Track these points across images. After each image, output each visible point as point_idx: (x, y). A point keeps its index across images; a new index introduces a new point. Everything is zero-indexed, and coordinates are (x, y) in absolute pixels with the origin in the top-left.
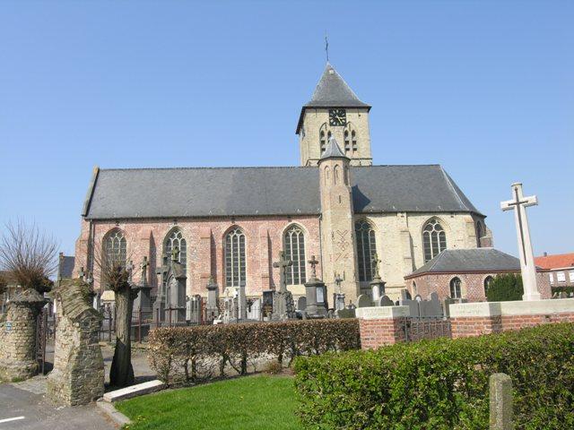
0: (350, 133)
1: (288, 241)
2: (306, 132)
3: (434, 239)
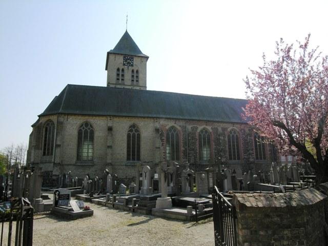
0: (135, 71)
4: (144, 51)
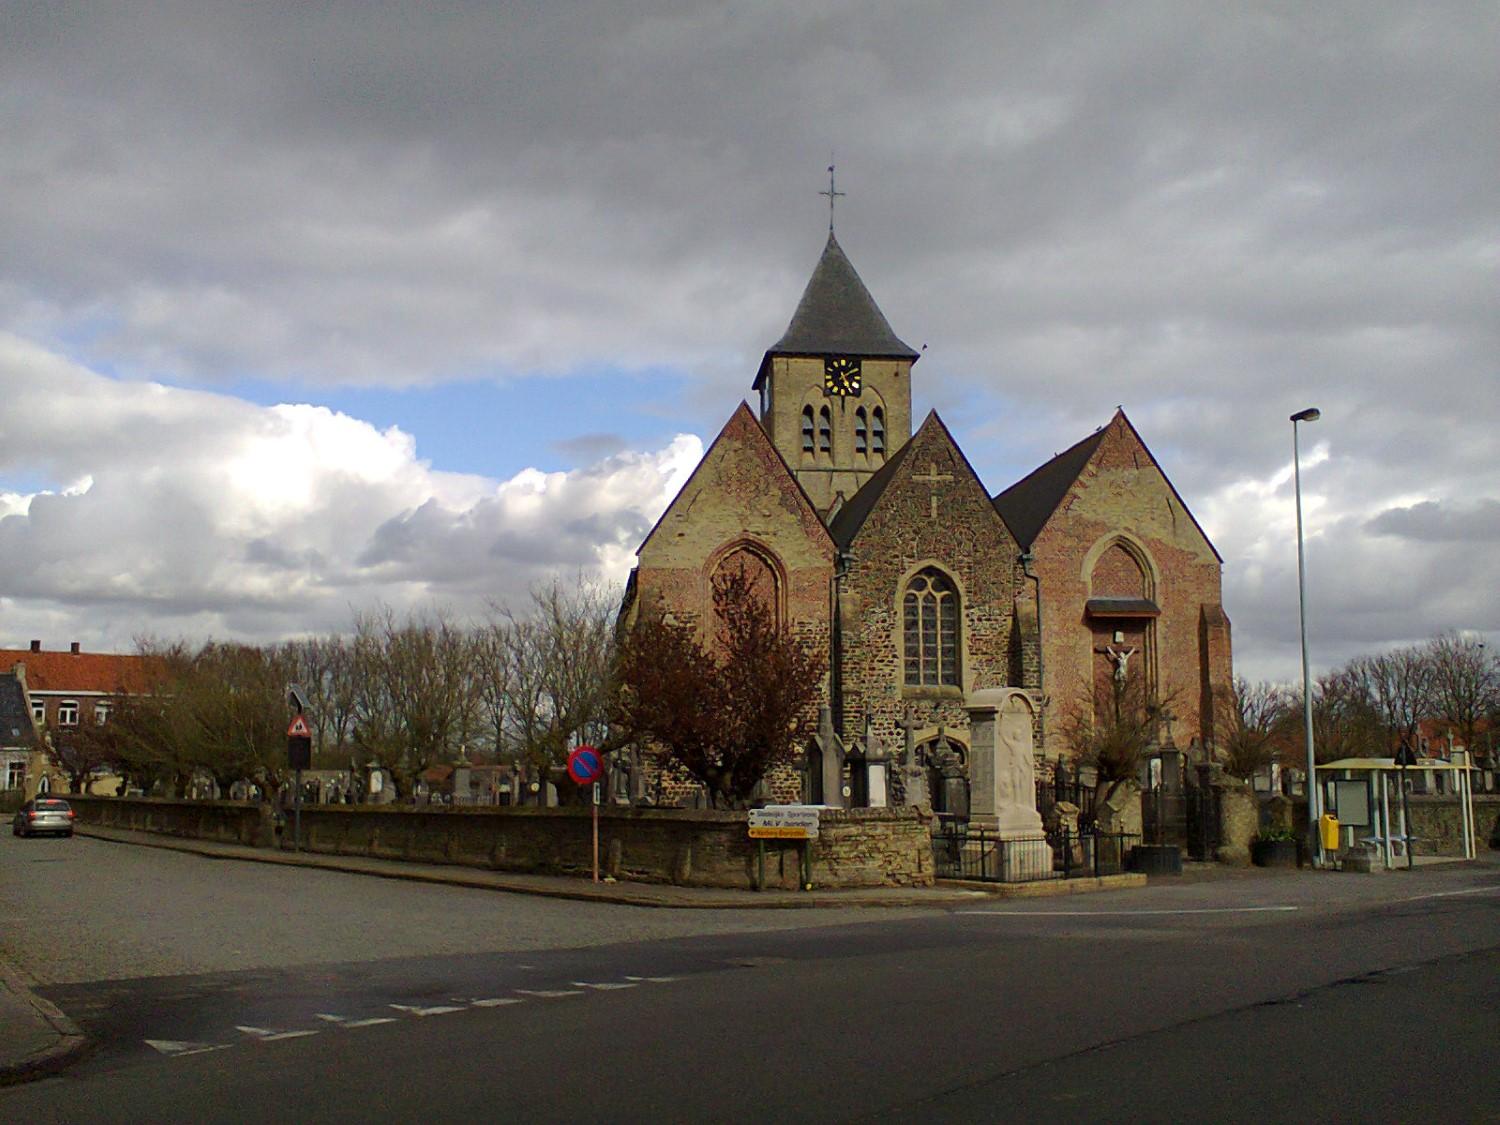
4: (907, 335)
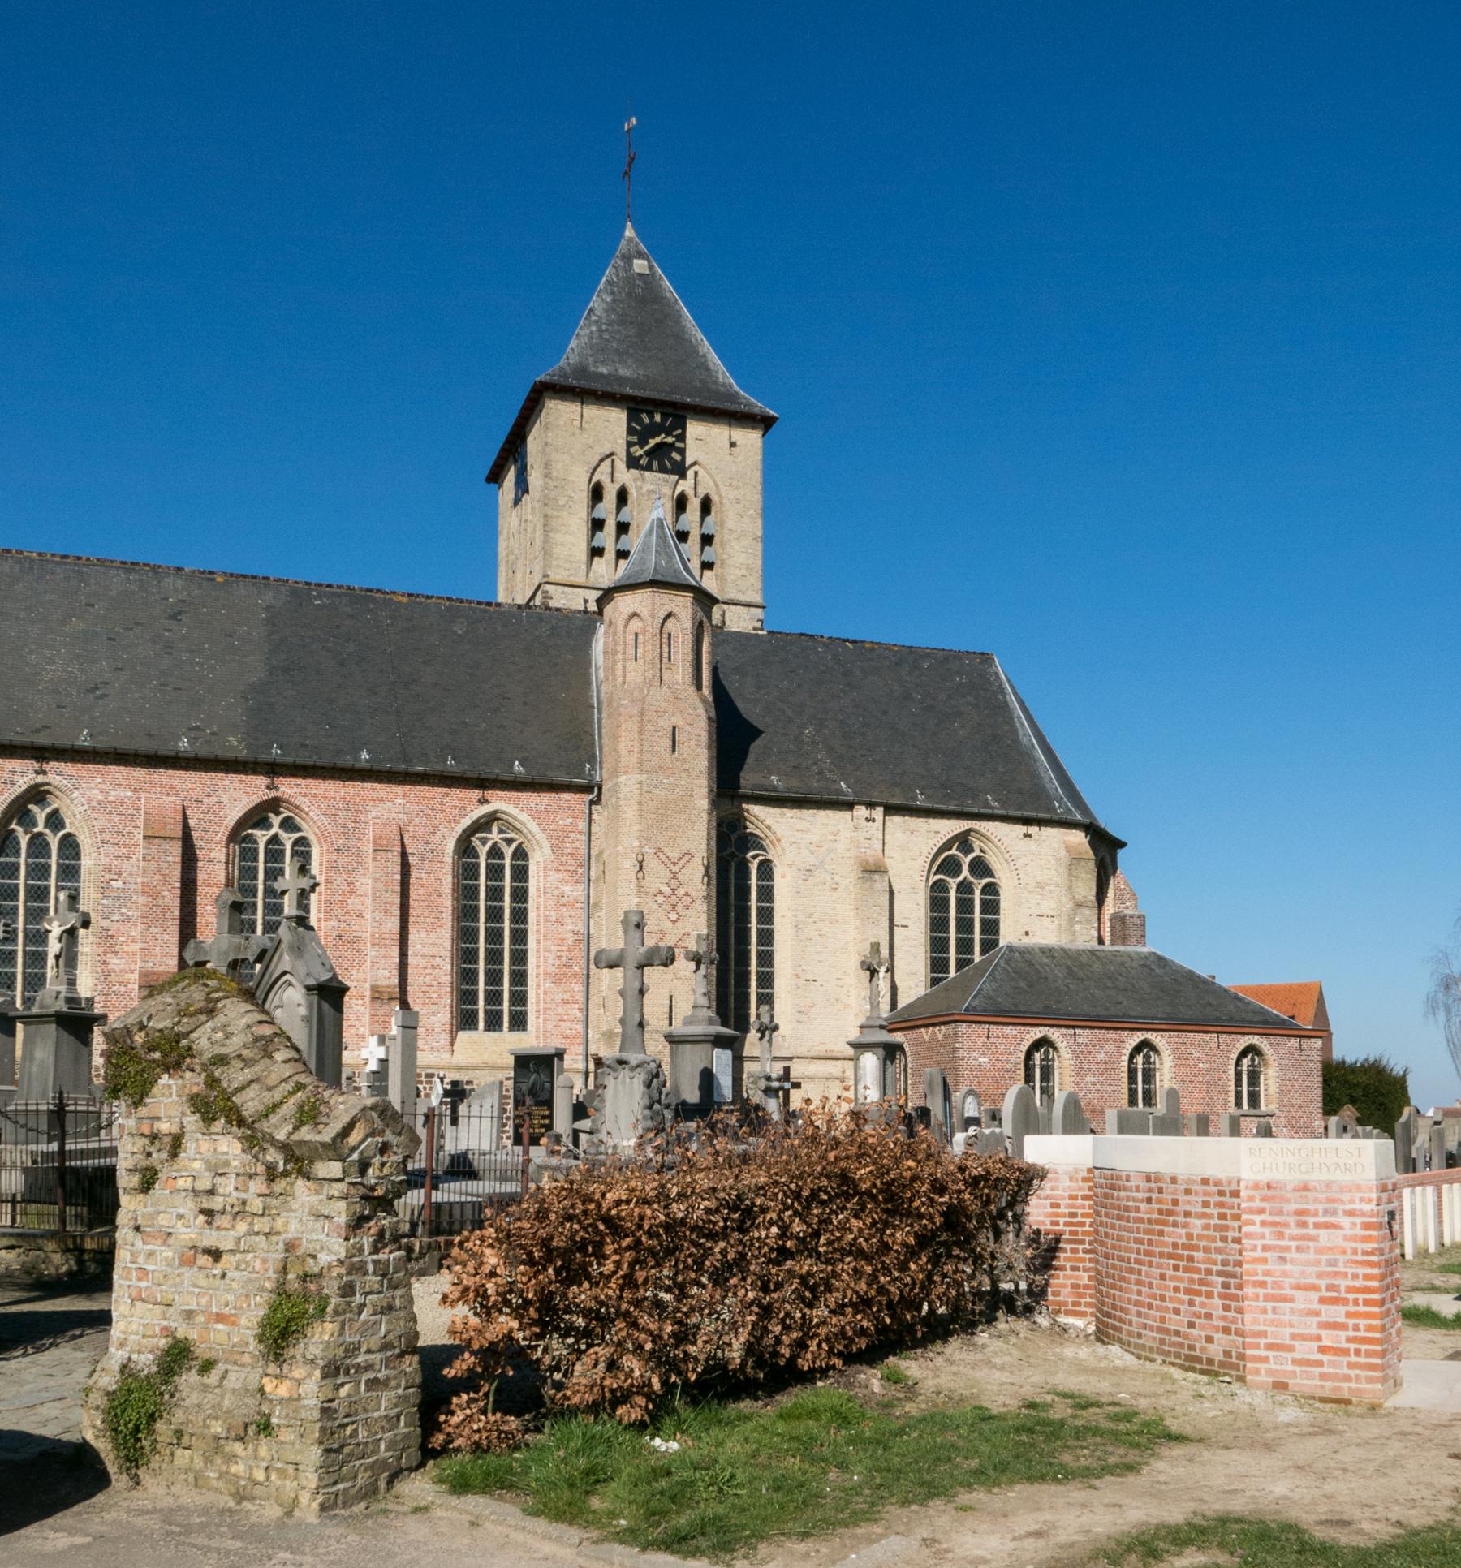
0: (694, 505)
1: (471, 871)
2: (534, 478)
3: (965, 905)
